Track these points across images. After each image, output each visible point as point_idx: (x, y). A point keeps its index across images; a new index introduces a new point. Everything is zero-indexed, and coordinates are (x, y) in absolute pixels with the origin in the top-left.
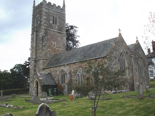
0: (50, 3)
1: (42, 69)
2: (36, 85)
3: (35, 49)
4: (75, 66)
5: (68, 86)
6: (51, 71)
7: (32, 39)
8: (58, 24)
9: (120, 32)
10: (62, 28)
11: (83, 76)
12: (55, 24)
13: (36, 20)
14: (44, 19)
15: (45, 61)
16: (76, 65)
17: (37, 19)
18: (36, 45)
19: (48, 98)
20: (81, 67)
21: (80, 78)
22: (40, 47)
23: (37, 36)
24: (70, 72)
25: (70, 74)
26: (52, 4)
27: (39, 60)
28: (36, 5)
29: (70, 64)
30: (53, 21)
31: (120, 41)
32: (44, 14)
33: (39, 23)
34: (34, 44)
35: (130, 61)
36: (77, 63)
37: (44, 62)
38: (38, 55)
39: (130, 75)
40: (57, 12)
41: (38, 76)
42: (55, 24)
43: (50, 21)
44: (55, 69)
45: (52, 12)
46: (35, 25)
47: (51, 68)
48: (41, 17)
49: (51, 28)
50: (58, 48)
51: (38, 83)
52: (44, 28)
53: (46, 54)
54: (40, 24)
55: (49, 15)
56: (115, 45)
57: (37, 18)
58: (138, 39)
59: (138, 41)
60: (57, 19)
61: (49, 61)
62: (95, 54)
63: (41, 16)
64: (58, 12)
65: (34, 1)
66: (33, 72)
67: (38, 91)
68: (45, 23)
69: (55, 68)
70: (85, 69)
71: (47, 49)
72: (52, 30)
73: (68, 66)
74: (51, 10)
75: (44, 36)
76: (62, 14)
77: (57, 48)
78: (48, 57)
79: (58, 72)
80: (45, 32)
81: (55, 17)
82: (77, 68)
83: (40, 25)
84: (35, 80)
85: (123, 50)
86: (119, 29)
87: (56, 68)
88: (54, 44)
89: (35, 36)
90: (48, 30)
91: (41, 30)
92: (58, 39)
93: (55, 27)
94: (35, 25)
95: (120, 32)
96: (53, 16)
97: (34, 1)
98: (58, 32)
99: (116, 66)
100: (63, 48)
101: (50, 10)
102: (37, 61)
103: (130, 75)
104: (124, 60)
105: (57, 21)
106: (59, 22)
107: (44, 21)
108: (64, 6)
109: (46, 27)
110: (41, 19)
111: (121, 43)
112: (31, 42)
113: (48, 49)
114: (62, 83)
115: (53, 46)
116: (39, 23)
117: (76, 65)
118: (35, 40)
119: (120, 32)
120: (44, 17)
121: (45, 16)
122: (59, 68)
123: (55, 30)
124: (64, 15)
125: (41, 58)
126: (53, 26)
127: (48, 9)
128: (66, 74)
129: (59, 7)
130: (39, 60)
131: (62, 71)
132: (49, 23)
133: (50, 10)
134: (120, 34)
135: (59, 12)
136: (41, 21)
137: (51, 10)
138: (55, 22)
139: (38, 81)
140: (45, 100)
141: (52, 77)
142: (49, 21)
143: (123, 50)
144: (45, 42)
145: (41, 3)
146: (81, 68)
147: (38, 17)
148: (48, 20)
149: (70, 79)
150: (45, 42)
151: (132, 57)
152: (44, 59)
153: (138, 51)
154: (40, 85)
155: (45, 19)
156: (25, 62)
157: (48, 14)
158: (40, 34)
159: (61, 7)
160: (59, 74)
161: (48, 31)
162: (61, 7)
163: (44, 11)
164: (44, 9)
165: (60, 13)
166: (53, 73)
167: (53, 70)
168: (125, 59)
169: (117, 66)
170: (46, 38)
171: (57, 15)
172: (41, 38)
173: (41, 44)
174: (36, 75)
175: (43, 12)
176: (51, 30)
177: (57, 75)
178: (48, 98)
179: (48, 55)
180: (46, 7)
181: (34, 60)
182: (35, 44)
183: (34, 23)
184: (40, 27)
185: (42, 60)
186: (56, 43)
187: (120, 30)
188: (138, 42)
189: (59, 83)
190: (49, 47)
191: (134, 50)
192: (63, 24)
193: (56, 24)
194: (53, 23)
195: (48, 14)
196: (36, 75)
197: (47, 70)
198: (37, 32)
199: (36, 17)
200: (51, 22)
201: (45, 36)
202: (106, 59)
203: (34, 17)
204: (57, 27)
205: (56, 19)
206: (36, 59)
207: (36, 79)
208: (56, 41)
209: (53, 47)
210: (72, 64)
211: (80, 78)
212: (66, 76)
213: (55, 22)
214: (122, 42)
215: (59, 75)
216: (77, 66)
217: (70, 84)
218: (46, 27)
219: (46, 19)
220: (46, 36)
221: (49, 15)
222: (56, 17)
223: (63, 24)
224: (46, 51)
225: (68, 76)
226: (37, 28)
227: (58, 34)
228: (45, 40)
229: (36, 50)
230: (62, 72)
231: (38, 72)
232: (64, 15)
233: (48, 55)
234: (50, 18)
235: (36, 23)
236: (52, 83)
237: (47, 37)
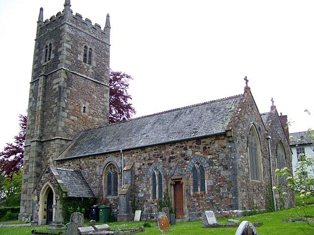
0: (79, 16)
1: (57, 161)
2: (47, 197)
3: (39, 116)
4: (145, 155)
5: (127, 200)
6: (80, 165)
7: (33, 93)
8: (94, 63)
9: (246, 83)
10: (103, 73)
11: (166, 177)
12: (87, 62)
13: (44, 51)
14: (65, 49)
15: (64, 142)
16: (146, 152)
17: (48, 48)
18: (42, 106)
19: (96, 226)
20: (161, 157)
21: (157, 181)
22: (55, 111)
23: (46, 85)
24: (132, 167)
25: (131, 172)
26: (84, 19)
27: (50, 140)
28: (47, 16)
29: (132, 151)
30: (85, 55)
31: (246, 101)
32: (66, 38)
33: (52, 56)
34: (39, 103)
35: (265, 148)
36: (149, 148)
37: (62, 146)
38: (46, 130)
39: (266, 176)
40: (94, 38)
41: (52, 175)
42: (87, 62)
43: (78, 55)
44: (93, 161)
45: (83, 35)
46: (42, 61)
47: (81, 160)
48: (59, 45)
49: (79, 72)
50: (93, 116)
51: (54, 191)
52: (65, 69)
53: (66, 127)
54: (54, 59)
55: (76, 42)
56: (240, 110)
57: (47, 46)
58: (275, 104)
59: (275, 107)
60: (93, 53)
61: (73, 144)
62: (194, 129)
63: (59, 42)
64: (96, 39)
65: (42, 9)
66: (34, 168)
67: (52, 213)
68: (67, 59)
69: (92, 159)
70: (170, 162)
71: (68, 117)
72: (81, 76)
73: (126, 154)
74: (83, 32)
75: (64, 88)
76: (102, 42)
77: (90, 117)
78: (71, 136)
79: (98, 168)
80: (66, 77)
81: (89, 47)
82: (150, 159)
83: (56, 62)
84: (43, 184)
85: (253, 123)
86: (246, 77)
87: (94, 158)
88: (84, 107)
89: (41, 86)
90: (73, 75)
91: (58, 72)
92: (93, 96)
93: (88, 69)
94: (42, 61)
95: (247, 85)
96: (85, 45)
97: (42, 9)
98: (94, 80)
99: (243, 155)
100: (103, 118)
101: (80, 31)
102: (45, 143)
103: (266, 176)
104: (255, 145)
105: (93, 58)
106: (97, 60)
107: (65, 52)
108: (108, 26)
109: (70, 67)
110: (57, 48)
111: (250, 108)
112: (30, 100)
113: (72, 117)
114: (109, 193)
115: (82, 111)
116: (52, 56)
117: (147, 154)
118: (40, 94)
119: (247, 85)
120: (66, 45)
121: (67, 42)
122: (101, 160)
123: (87, 75)
124: (107, 46)
125: (55, 136)
126: (83, 67)
127: (75, 28)
128: (121, 174)
129: (97, 28)
130: (50, 140)
131: (111, 165)
132: (76, 59)
133: (80, 31)
134: (247, 89)
135: (97, 38)
136: (57, 54)
137: (83, 32)
138: (87, 58)
139: (52, 188)
140: (103, 228)
141: (84, 179)
142: (77, 53)
143: (253, 123)
144: (66, 101)
145: (58, 14)
146: (159, 159)
147: (51, 44)
148: (74, 51)
149: (131, 185)
150: (66, 101)
151: (268, 139)
152: (61, 139)
153: (276, 127)
154: (57, 198)
155: (68, 49)
156: (6, 146)
157: (75, 40)
158: (55, 81)
159: (102, 29)
160: (101, 173)
161: (74, 76)
162: (102, 29)
163: (67, 33)
164: (67, 26)
165: (99, 40)
166: (87, 169)
167: (86, 164)
168: (257, 143)
169: (245, 155)
170: (69, 91)
171: (93, 44)
172: (57, 90)
173: (56, 103)
174: (48, 174)
175: (63, 33)
176: (80, 74)
177: (96, 175)
178: (96, 226)
179: (71, 131)
180: (71, 24)
181: (37, 141)
182: (40, 104)
183: (40, 58)
184: (55, 66)
185: (57, 141)
186: (88, 104)
187: (246, 79)
188: (276, 110)
189: (100, 194)
190: (73, 112)
191: (269, 125)
192: (104, 66)
193: (90, 63)
194: (85, 61)
195: (75, 40)
196: (47, 173)
197: (71, 164)
198: (46, 77)
199: (45, 44)
200: (81, 58)
201: (66, 86)
202: (224, 139)
203: (39, 44)
204: (91, 70)
205: (90, 53)
206: (41, 138)
207: (48, 183)
208: (88, 101)
209: (83, 113)
210: (135, 151)
211: (157, 181)
212: (121, 178)
213: (87, 58)
214: (251, 106)
215: (102, 176)
216: (149, 154)
217: (132, 196)
218: (70, 67)
219: (69, 49)
220: (68, 86)
221: (76, 42)
222: (90, 49)
223: (104, 66)
224: (67, 120)
225: (126, 176)
226: (47, 69)
227: (93, 86)
228: (66, 96)
229: (43, 118)
230: (109, 169)
231: (52, 165)
232: (107, 46)
233: (71, 131)
234: (79, 49)
235: (44, 57)
236: (83, 193)
237: (71, 90)
